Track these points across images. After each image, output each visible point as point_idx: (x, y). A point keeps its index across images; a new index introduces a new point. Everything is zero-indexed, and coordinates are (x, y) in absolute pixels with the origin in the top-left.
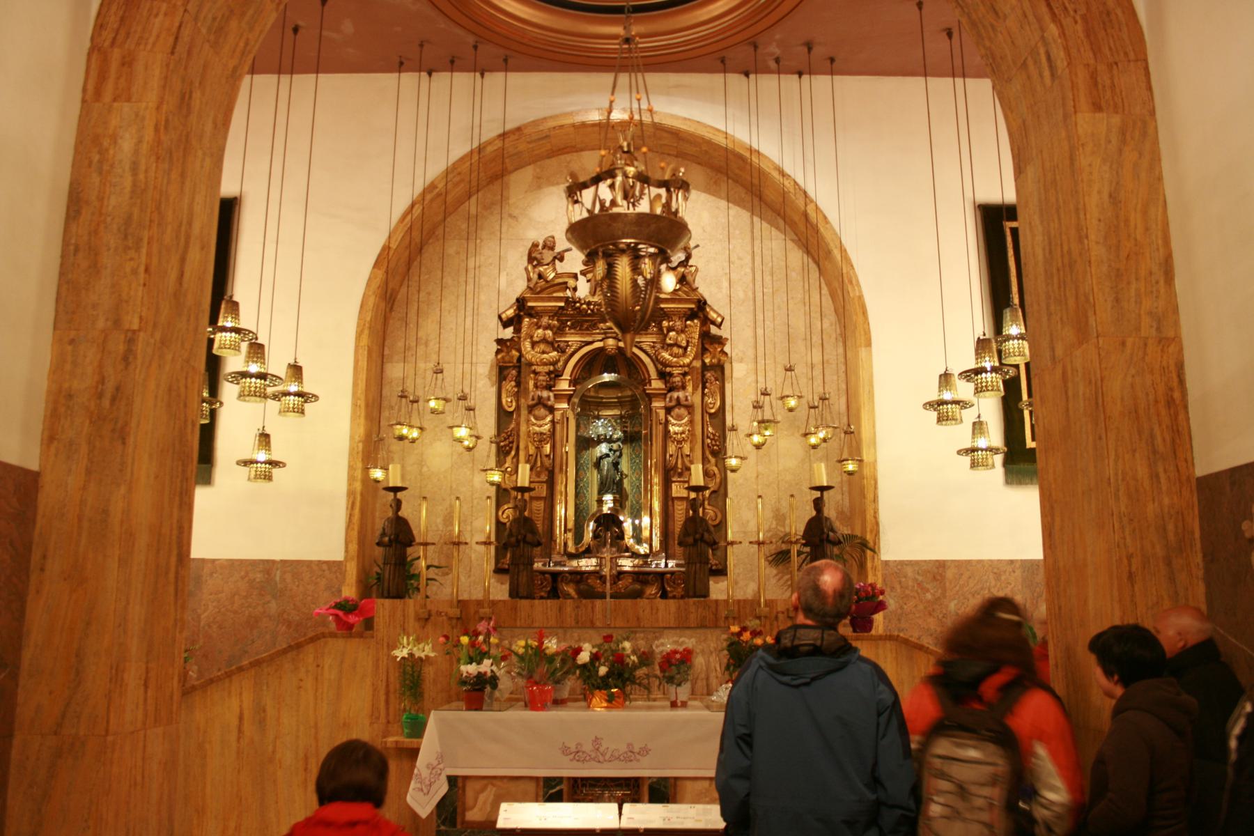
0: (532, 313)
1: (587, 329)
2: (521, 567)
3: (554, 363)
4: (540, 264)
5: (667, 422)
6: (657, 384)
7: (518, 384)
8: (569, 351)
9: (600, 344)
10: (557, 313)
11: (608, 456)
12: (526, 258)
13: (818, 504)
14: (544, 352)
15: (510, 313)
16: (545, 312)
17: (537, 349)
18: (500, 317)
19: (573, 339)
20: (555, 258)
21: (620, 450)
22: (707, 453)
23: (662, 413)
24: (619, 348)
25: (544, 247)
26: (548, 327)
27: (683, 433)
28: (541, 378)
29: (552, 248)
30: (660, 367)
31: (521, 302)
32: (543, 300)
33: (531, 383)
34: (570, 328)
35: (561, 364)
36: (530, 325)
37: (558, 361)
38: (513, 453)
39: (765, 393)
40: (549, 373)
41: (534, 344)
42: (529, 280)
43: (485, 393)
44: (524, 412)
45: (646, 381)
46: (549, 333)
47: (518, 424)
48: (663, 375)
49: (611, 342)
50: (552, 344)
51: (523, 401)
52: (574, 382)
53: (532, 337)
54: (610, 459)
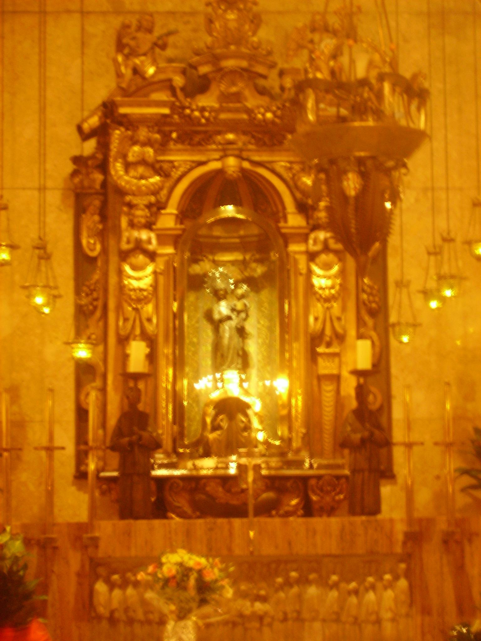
0: (128, 123)
1: (199, 144)
2: (136, 478)
3: (155, 193)
4: (133, 53)
5: (310, 273)
6: (295, 220)
7: (104, 218)
8: (175, 174)
9: (215, 165)
10: (160, 123)
11: (229, 318)
12: (113, 48)
14: (142, 177)
15: (94, 121)
16: (144, 120)
17: (132, 173)
18: (79, 128)
19: (179, 157)
20: (155, 44)
21: (246, 310)
22: (363, 312)
23: (302, 261)
24: (243, 170)
25: (139, 28)
26: (149, 143)
27: (333, 287)
28: (139, 213)
29: (150, 31)
30: (298, 195)
31: (108, 109)
32: (140, 105)
33: (124, 222)
34: (176, 141)
35: (164, 192)
36: (122, 140)
37: (161, 189)
38: (98, 314)
39: (448, 240)
40: (149, 206)
41: (128, 166)
42: (119, 75)
43: (60, 226)
44: (114, 259)
45: (279, 215)
46: (150, 151)
47: (106, 275)
48: (303, 208)
49: (232, 161)
50: (156, 168)
51: (112, 243)
52: (183, 215)
53: (125, 156)
54: (233, 323)
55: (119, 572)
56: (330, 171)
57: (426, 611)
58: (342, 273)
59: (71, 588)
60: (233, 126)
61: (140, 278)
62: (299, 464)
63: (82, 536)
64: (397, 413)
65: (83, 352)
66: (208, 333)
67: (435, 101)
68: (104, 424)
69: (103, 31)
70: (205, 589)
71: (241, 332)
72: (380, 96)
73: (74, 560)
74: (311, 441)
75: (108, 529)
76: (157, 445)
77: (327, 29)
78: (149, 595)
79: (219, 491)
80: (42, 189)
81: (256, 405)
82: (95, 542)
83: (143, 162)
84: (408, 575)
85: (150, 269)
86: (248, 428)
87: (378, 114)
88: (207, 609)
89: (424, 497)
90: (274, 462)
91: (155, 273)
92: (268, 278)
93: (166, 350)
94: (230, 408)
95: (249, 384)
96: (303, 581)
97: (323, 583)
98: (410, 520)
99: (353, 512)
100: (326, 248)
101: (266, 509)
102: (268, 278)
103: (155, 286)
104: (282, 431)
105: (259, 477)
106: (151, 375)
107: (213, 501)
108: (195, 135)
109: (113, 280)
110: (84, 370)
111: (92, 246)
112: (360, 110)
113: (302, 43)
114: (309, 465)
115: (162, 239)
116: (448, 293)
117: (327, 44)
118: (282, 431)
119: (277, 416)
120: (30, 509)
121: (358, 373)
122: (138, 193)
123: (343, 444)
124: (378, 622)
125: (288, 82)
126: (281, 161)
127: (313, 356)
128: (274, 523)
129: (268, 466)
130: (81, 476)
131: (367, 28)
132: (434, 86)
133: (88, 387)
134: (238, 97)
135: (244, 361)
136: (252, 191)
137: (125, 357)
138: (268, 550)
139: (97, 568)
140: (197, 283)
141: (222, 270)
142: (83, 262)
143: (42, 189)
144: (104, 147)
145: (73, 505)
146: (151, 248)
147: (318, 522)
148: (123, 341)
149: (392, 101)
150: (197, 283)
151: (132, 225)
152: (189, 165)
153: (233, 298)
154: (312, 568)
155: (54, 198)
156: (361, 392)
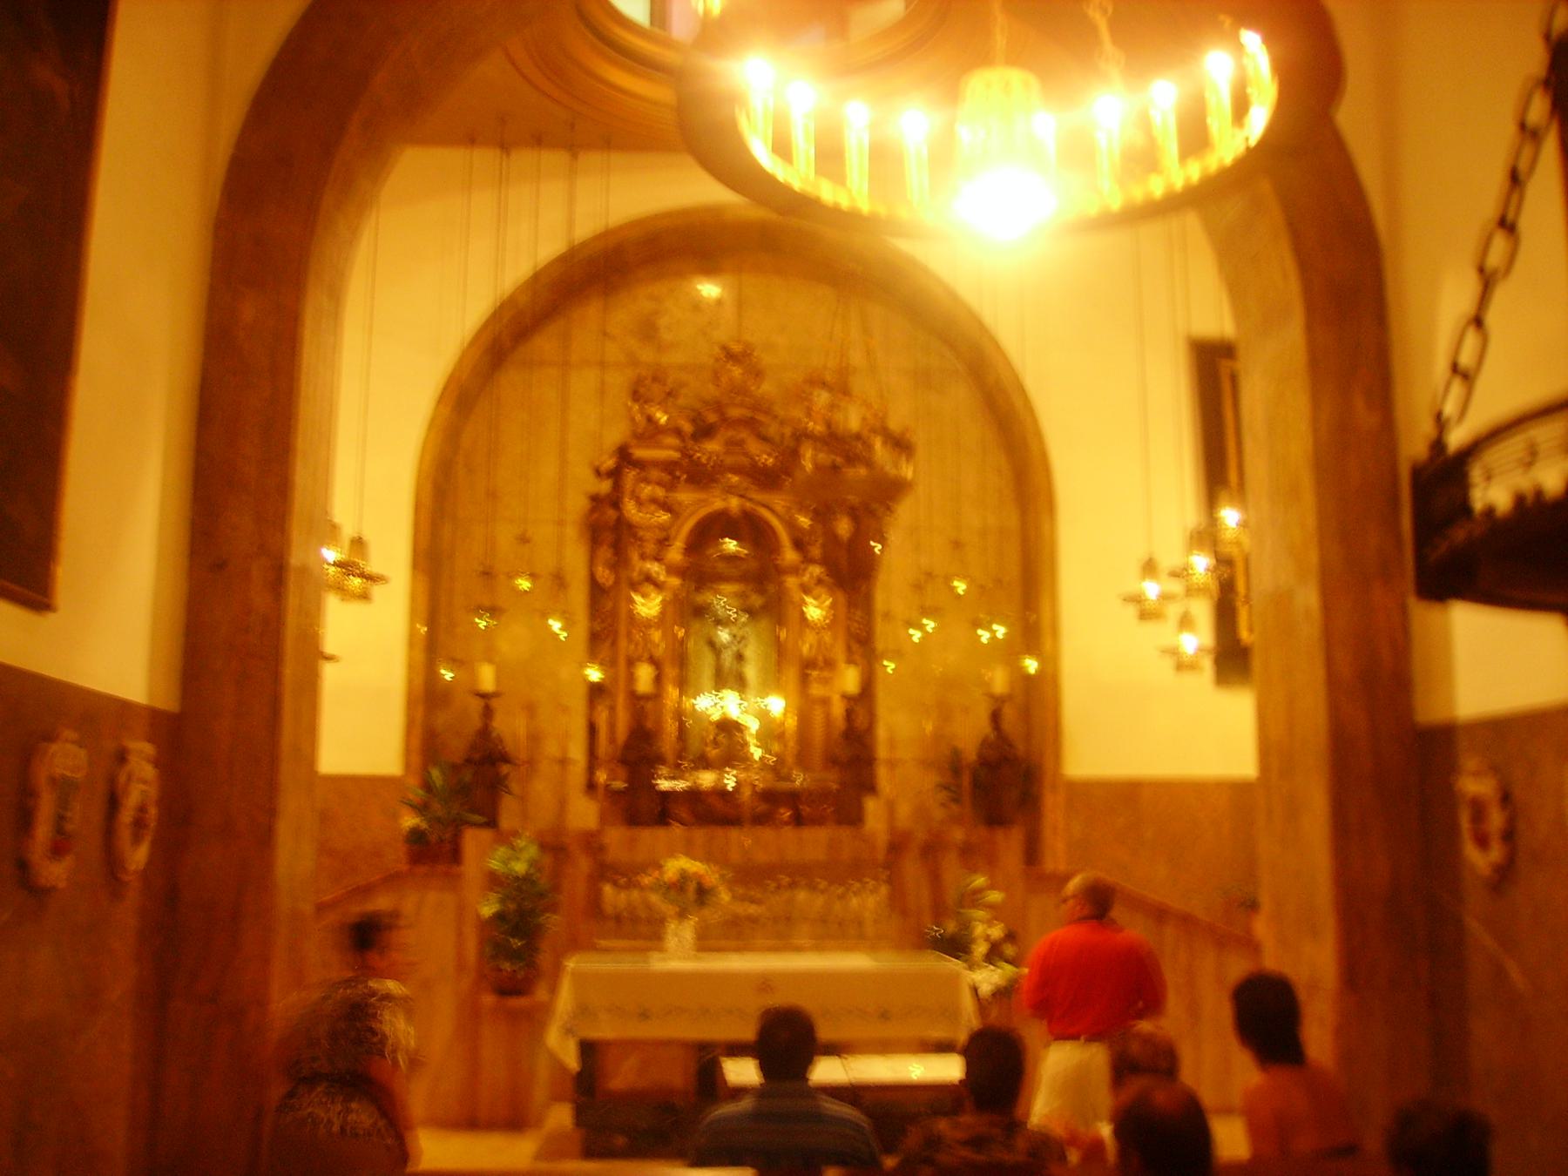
0: (640, 465)
3: (662, 527)
6: (790, 555)
10: (669, 467)
13: (996, 717)
15: (610, 463)
16: (656, 464)
19: (685, 496)
26: (659, 484)
31: (624, 455)
43: (575, 558)
48: (799, 545)
50: (666, 506)
55: (626, 875)
56: (823, 515)
57: (904, 913)
58: (833, 606)
59: (581, 888)
60: (736, 470)
61: (648, 606)
62: (788, 778)
63: (591, 843)
64: (882, 733)
65: (594, 674)
66: (708, 659)
67: (921, 453)
68: (612, 740)
69: (619, 381)
70: (703, 894)
71: (740, 657)
72: (869, 447)
73: (583, 865)
74: (802, 759)
75: (615, 837)
76: (661, 760)
77: (824, 385)
78: (654, 898)
79: (719, 805)
80: (561, 523)
81: (752, 725)
82: (602, 849)
83: (654, 501)
84: (889, 881)
85: (659, 599)
86: (745, 744)
87: (869, 464)
88: (706, 912)
89: (904, 811)
90: (770, 776)
91: (663, 602)
92: (766, 608)
93: (671, 672)
94: (728, 728)
95: (748, 708)
96: (793, 885)
97: (812, 887)
98: (892, 830)
99: (839, 822)
100: (820, 582)
101: (760, 820)
102: (766, 608)
103: (663, 613)
104: (776, 747)
105: (755, 792)
106: (657, 696)
107: (710, 811)
108: (701, 476)
109: (623, 604)
110: (596, 691)
111: (604, 575)
112: (852, 459)
113: (800, 396)
114: (799, 780)
115: (671, 570)
116: (930, 625)
117: (822, 398)
118: (776, 747)
119: (771, 733)
120: (543, 816)
121: (847, 698)
122: (649, 528)
123: (831, 761)
124: (860, 924)
125: (788, 431)
126: (779, 501)
127: (804, 680)
128: (767, 834)
129: (760, 781)
130: (591, 786)
131: (859, 384)
132: (919, 438)
133: (600, 708)
134: (740, 443)
135: (740, 684)
136: (751, 528)
137: (631, 678)
138: (761, 857)
139: (604, 871)
140: (700, 612)
141: (723, 600)
142: (597, 591)
143: (561, 523)
144: (617, 487)
145: (584, 813)
146: (474, 841)
147: (808, 834)
148: (631, 663)
149: (880, 450)
150: (700, 612)
151: (643, 557)
152: (696, 504)
153: (731, 626)
154: (802, 874)
155: (572, 532)
156: (849, 715)
